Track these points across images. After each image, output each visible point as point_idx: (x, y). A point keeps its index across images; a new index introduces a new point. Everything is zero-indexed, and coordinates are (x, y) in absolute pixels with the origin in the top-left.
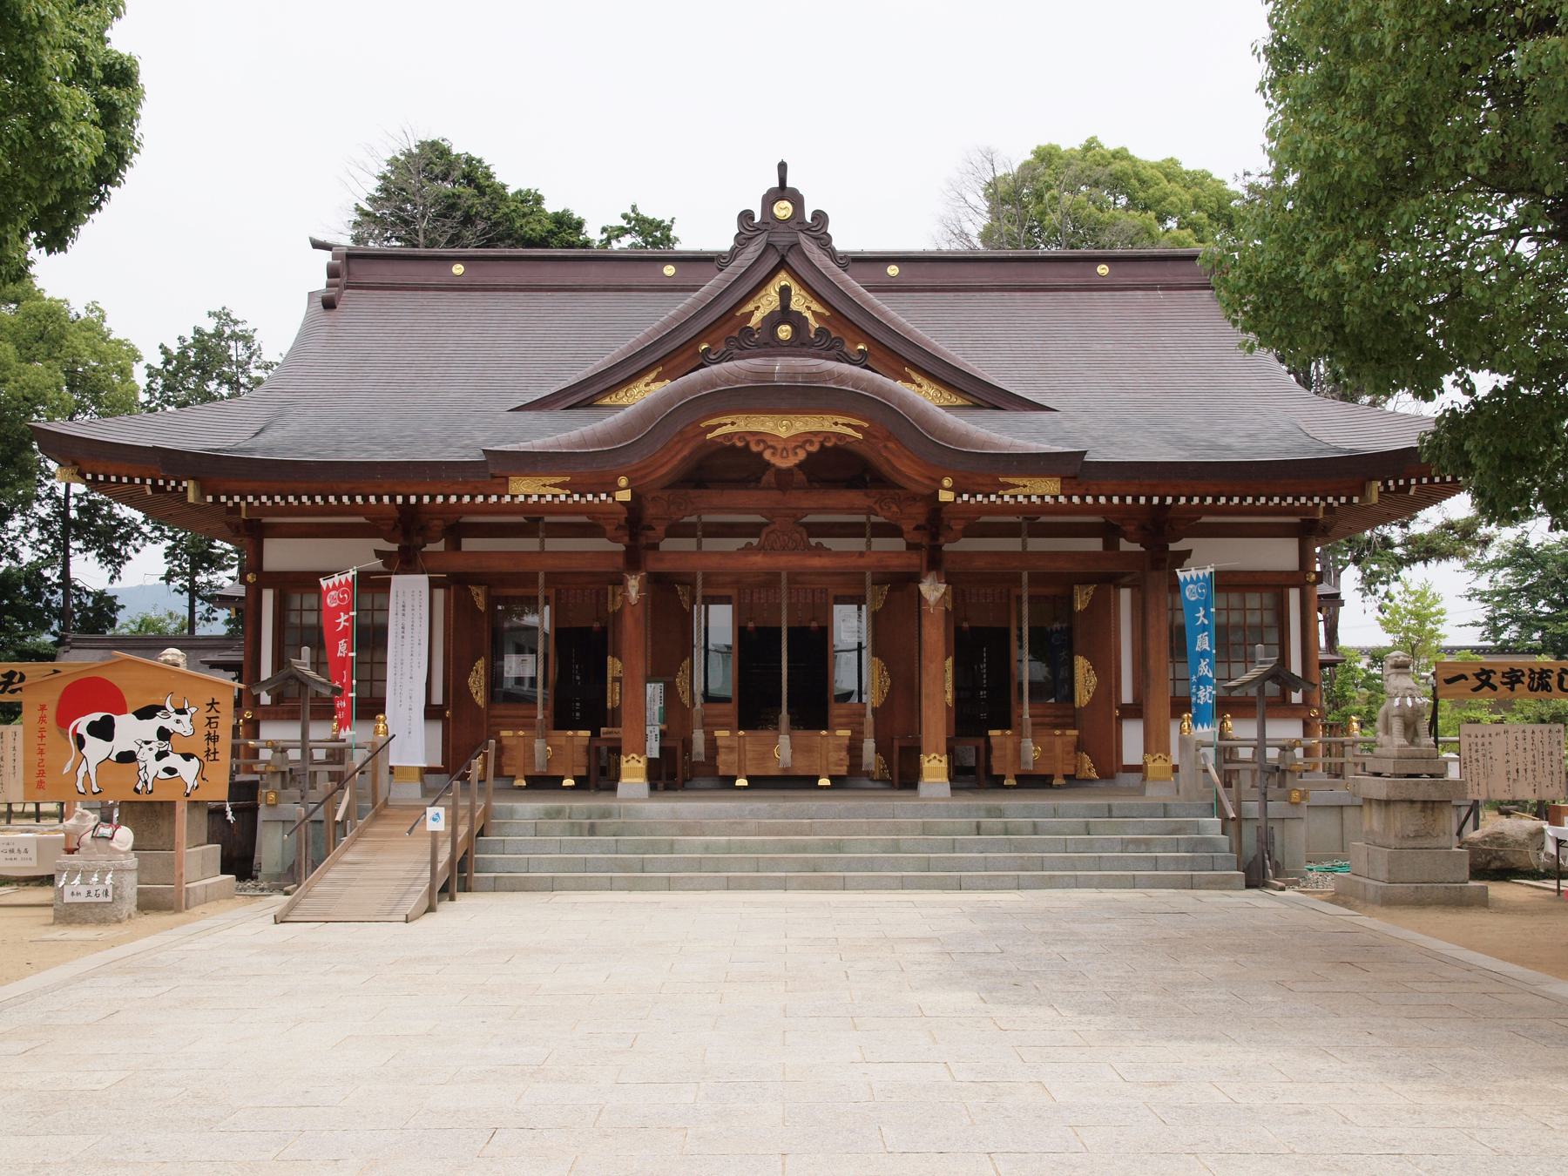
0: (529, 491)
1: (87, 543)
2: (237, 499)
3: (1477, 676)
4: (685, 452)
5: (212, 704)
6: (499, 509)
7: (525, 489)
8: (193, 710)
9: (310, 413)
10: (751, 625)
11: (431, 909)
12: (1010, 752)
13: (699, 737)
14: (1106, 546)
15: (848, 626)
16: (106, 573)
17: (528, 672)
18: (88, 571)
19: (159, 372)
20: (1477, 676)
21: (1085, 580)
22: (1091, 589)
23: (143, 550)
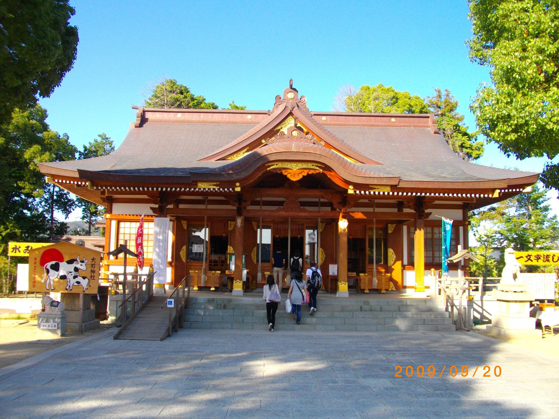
0: (205, 187)
1: (59, 207)
2: (104, 188)
3: (527, 257)
4: (260, 174)
5: (93, 259)
6: (193, 194)
7: (203, 186)
8: (86, 261)
9: (129, 161)
10: (277, 236)
11: (169, 336)
12: (367, 281)
13: (259, 275)
14: (399, 211)
15: (310, 236)
16: (64, 216)
17: (202, 251)
18: (59, 216)
19: (83, 154)
20: (527, 257)
21: (392, 222)
22: (394, 225)
23: (75, 209)
